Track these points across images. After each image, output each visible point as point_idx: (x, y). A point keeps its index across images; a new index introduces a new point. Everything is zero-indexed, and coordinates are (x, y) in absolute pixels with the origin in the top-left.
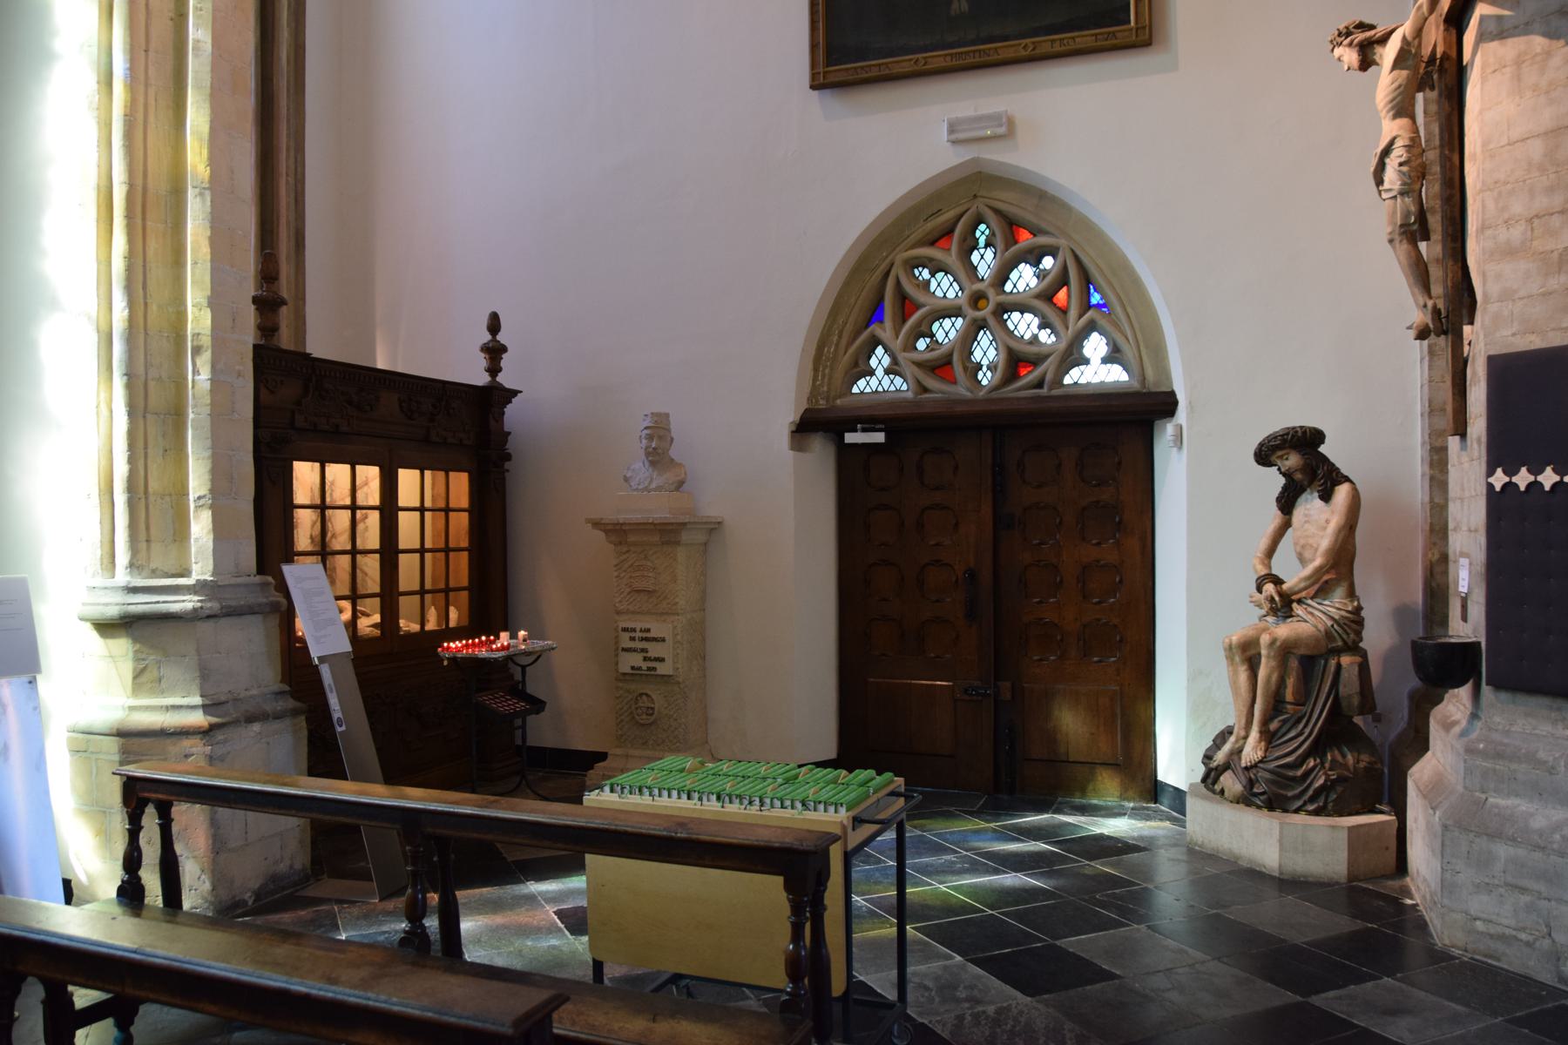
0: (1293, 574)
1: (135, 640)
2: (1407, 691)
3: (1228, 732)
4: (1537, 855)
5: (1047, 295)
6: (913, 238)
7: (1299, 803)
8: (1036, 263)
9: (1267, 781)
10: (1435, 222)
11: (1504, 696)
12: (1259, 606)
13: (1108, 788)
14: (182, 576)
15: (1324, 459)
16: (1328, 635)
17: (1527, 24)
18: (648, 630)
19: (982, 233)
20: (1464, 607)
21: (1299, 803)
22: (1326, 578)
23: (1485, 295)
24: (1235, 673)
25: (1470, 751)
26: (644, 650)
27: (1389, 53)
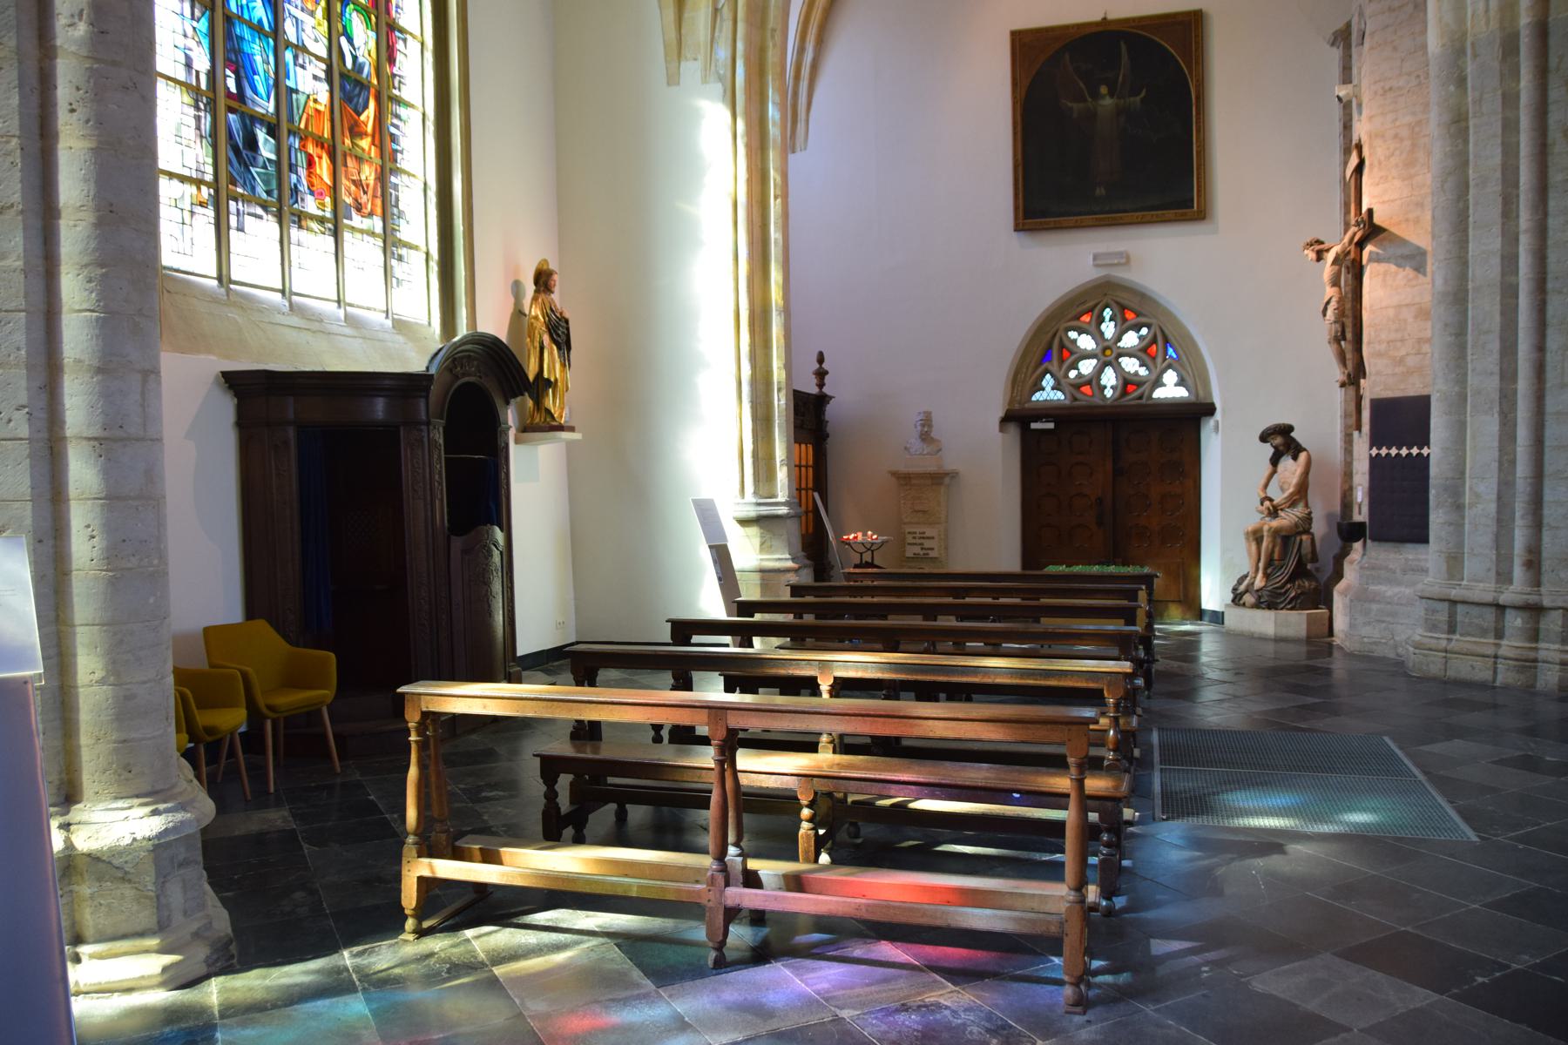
0: (1278, 497)
1: (761, 528)
2: (1332, 556)
3: (1246, 576)
4: (1389, 606)
5: (1145, 350)
6: (1070, 316)
7: (1282, 606)
8: (1138, 331)
9: (1268, 596)
10: (1349, 335)
11: (1376, 543)
12: (1262, 512)
13: (1174, 611)
14: (770, 498)
15: (1293, 440)
16: (1296, 525)
17: (1389, 258)
18: (924, 533)
19: (1107, 313)
20: (1360, 508)
21: (1282, 606)
22: (1295, 498)
23: (1370, 373)
24: (1250, 546)
25: (1361, 568)
26: (921, 544)
27: (1330, 256)
